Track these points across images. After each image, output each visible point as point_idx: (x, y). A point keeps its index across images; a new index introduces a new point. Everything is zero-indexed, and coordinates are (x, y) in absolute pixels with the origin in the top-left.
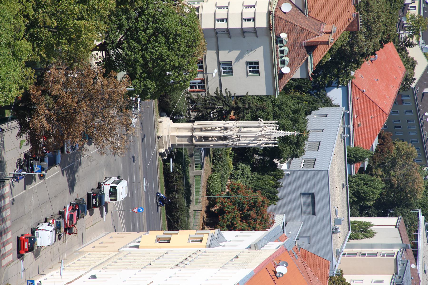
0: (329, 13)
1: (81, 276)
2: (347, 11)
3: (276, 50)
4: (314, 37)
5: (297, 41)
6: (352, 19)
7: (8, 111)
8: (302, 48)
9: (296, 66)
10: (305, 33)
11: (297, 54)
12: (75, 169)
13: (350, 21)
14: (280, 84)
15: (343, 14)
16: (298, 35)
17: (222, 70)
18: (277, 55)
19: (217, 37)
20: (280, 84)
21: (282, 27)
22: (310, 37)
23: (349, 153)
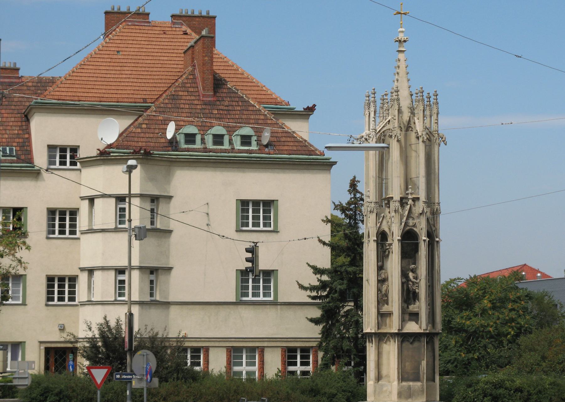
0: (160, 66)
1: (86, 47)
2: (165, 36)
3: (210, 152)
4: (195, 78)
5: (198, 111)
6: (184, 28)
7: (359, 232)
8: (218, 103)
9: (262, 117)
10: (180, 93)
11: (231, 112)
12: (362, 306)
13: (189, 31)
14: (303, 152)
15: (170, 44)
16: (182, 106)
17: (250, 298)
18: (225, 151)
19: (167, 304)
20: (303, 152)
21: (152, 135)
22: (196, 90)
23: (427, 153)
